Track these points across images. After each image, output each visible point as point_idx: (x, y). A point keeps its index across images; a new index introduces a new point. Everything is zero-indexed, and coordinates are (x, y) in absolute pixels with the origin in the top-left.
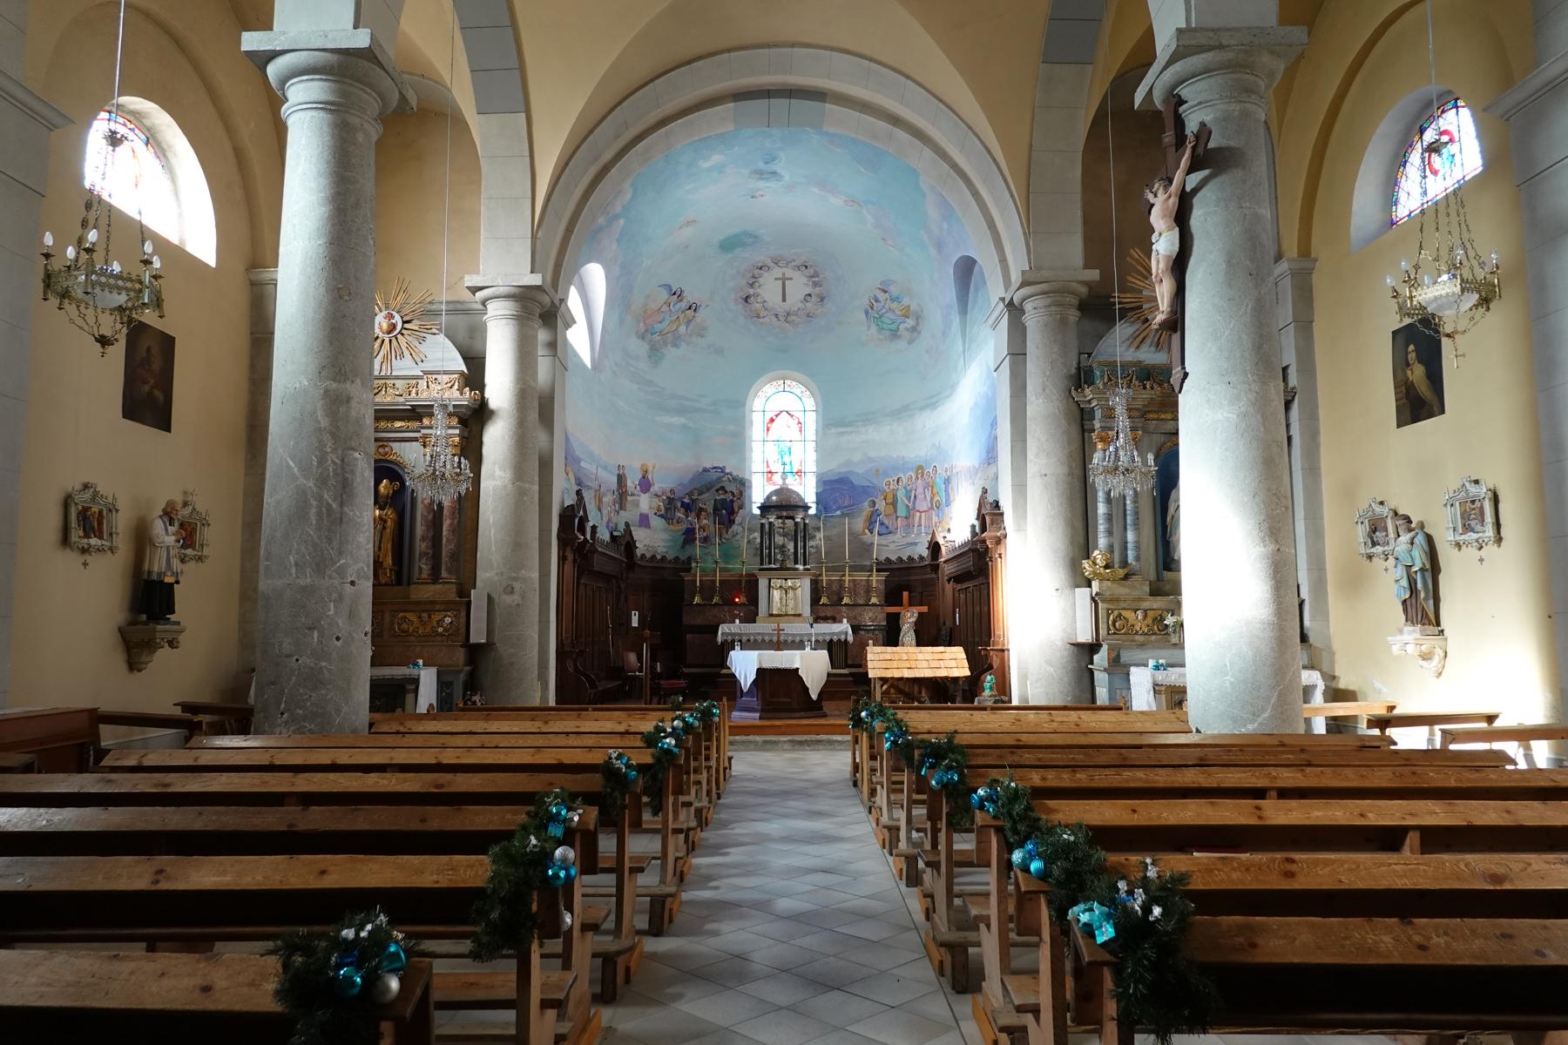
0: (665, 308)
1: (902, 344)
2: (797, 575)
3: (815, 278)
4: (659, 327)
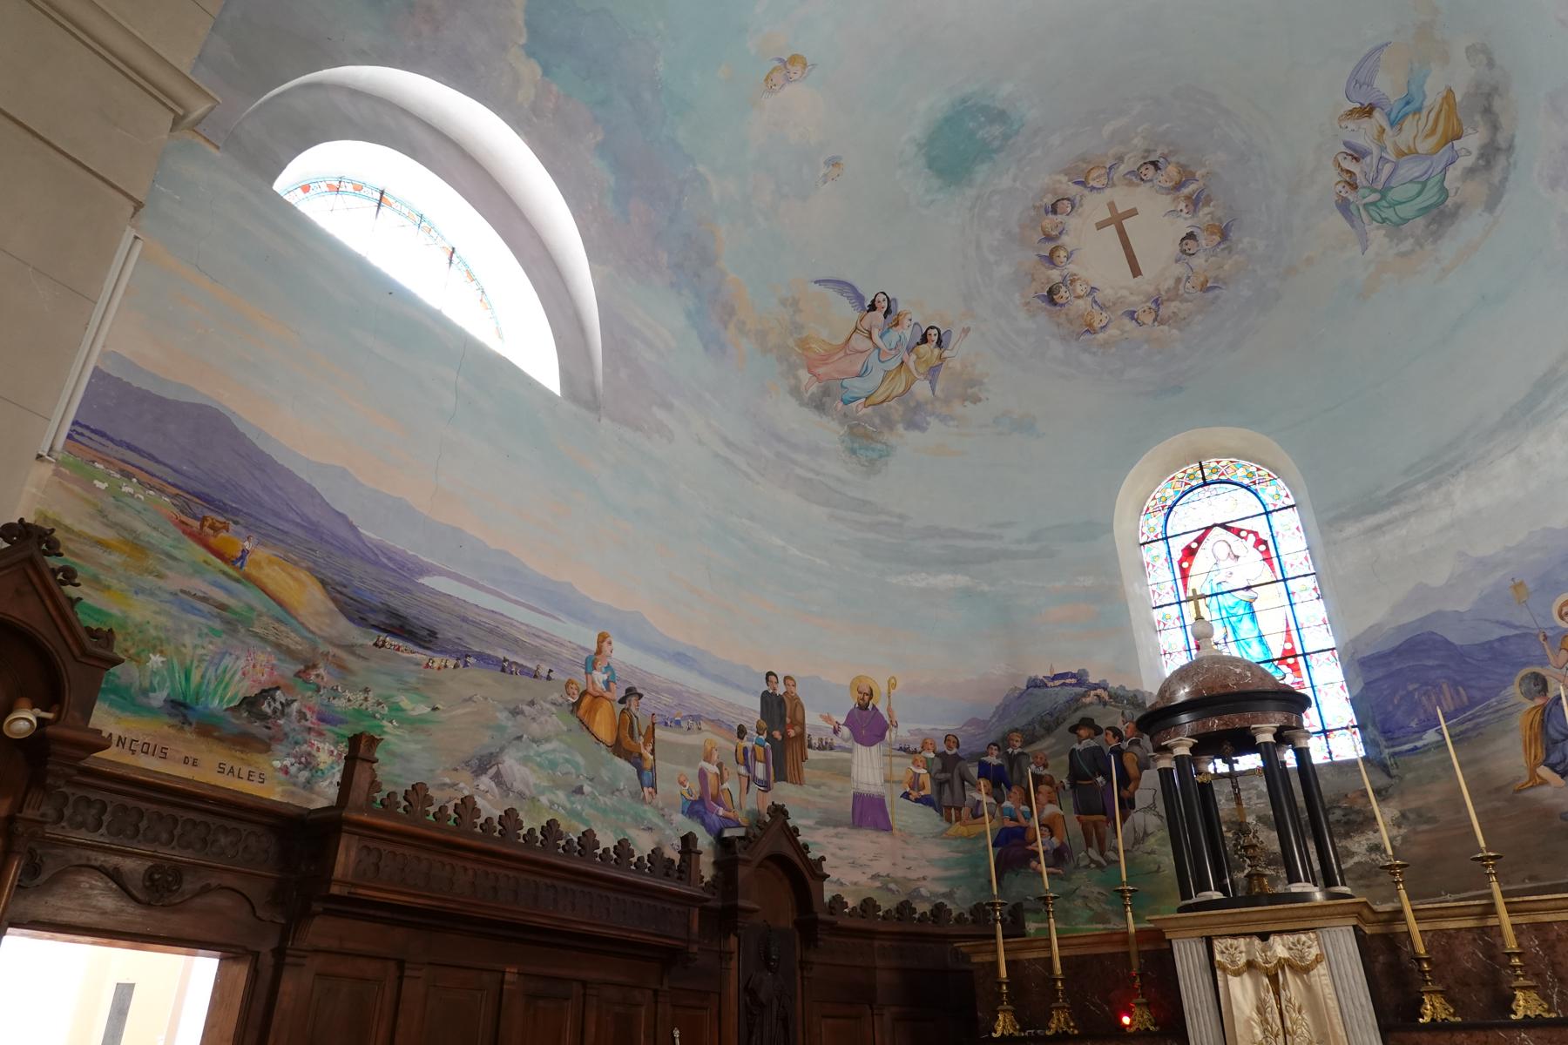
0: (860, 342)
1: (1471, 226)
2: (1304, 920)
3: (1189, 189)
4: (858, 386)
